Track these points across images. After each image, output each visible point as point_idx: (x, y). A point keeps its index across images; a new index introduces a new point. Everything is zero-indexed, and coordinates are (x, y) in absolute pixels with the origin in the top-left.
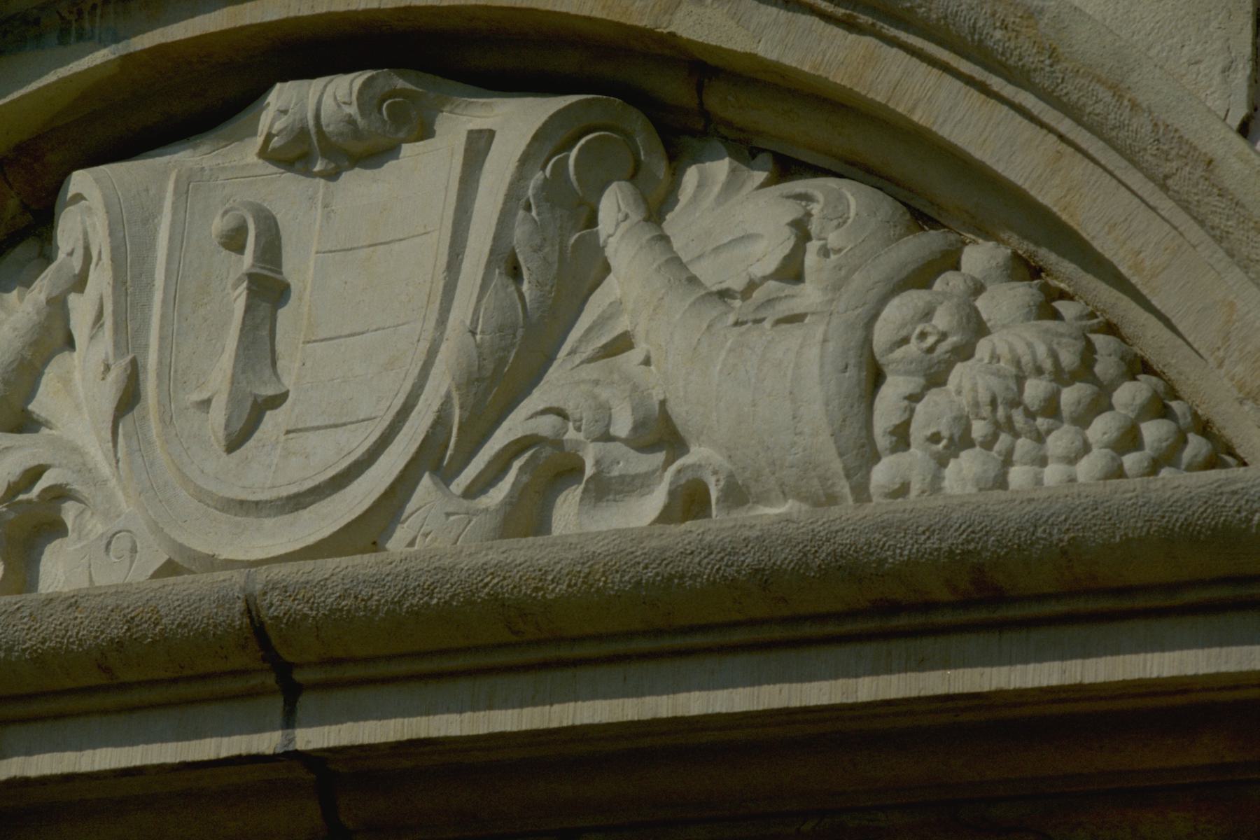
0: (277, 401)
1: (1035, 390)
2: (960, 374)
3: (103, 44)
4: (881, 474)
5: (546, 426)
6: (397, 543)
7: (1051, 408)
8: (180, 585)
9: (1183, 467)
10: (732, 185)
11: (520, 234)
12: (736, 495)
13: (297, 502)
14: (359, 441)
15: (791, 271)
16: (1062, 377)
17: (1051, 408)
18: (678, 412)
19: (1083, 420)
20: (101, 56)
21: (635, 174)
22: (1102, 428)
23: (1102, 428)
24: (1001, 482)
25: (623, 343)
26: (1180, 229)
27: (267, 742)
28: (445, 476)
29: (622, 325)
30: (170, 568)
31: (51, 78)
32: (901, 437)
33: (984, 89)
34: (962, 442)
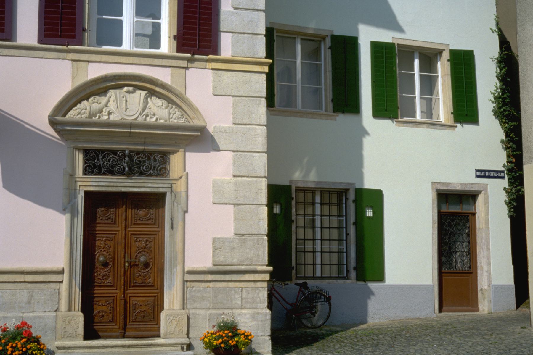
0: (128, 109)
1: (180, 116)
2: (175, 115)
3: (114, 82)
4: (171, 120)
5: (147, 113)
6: (67, 116)
7: (181, 117)
8: (123, 121)
9: (446, 56)
10: (156, 99)
11: (144, 100)
12: (160, 119)
13: (131, 116)
14: (135, 113)
15: (162, 106)
16: (181, 116)
17: (181, 117)
18: (155, 114)
19: (182, 118)
20: (114, 83)
21: (150, 97)
22: (183, 119)
23: (183, 119)
24: (145, 120)
25: (150, 108)
26: (211, 308)
27: (129, 130)
28: (141, 115)
29: (150, 107)
30: (121, 119)
31: (110, 84)
32: (172, 118)
33: (176, 97)
34: (176, 119)
